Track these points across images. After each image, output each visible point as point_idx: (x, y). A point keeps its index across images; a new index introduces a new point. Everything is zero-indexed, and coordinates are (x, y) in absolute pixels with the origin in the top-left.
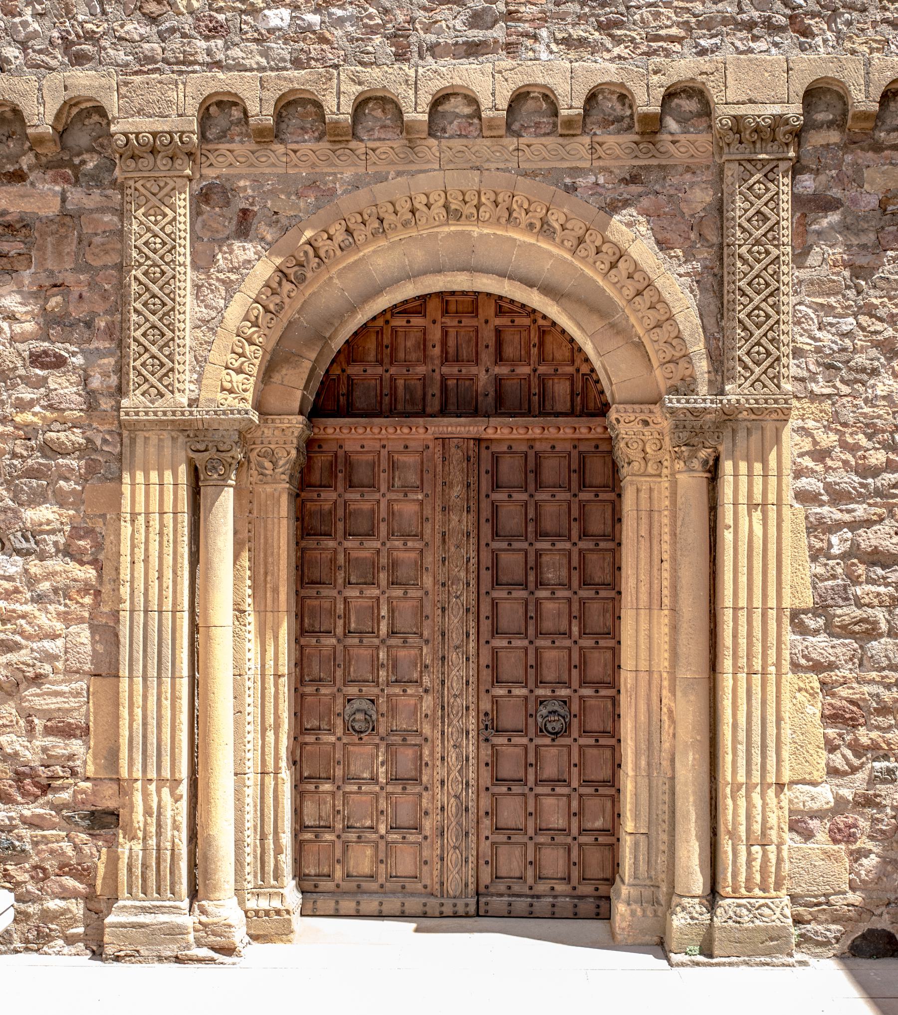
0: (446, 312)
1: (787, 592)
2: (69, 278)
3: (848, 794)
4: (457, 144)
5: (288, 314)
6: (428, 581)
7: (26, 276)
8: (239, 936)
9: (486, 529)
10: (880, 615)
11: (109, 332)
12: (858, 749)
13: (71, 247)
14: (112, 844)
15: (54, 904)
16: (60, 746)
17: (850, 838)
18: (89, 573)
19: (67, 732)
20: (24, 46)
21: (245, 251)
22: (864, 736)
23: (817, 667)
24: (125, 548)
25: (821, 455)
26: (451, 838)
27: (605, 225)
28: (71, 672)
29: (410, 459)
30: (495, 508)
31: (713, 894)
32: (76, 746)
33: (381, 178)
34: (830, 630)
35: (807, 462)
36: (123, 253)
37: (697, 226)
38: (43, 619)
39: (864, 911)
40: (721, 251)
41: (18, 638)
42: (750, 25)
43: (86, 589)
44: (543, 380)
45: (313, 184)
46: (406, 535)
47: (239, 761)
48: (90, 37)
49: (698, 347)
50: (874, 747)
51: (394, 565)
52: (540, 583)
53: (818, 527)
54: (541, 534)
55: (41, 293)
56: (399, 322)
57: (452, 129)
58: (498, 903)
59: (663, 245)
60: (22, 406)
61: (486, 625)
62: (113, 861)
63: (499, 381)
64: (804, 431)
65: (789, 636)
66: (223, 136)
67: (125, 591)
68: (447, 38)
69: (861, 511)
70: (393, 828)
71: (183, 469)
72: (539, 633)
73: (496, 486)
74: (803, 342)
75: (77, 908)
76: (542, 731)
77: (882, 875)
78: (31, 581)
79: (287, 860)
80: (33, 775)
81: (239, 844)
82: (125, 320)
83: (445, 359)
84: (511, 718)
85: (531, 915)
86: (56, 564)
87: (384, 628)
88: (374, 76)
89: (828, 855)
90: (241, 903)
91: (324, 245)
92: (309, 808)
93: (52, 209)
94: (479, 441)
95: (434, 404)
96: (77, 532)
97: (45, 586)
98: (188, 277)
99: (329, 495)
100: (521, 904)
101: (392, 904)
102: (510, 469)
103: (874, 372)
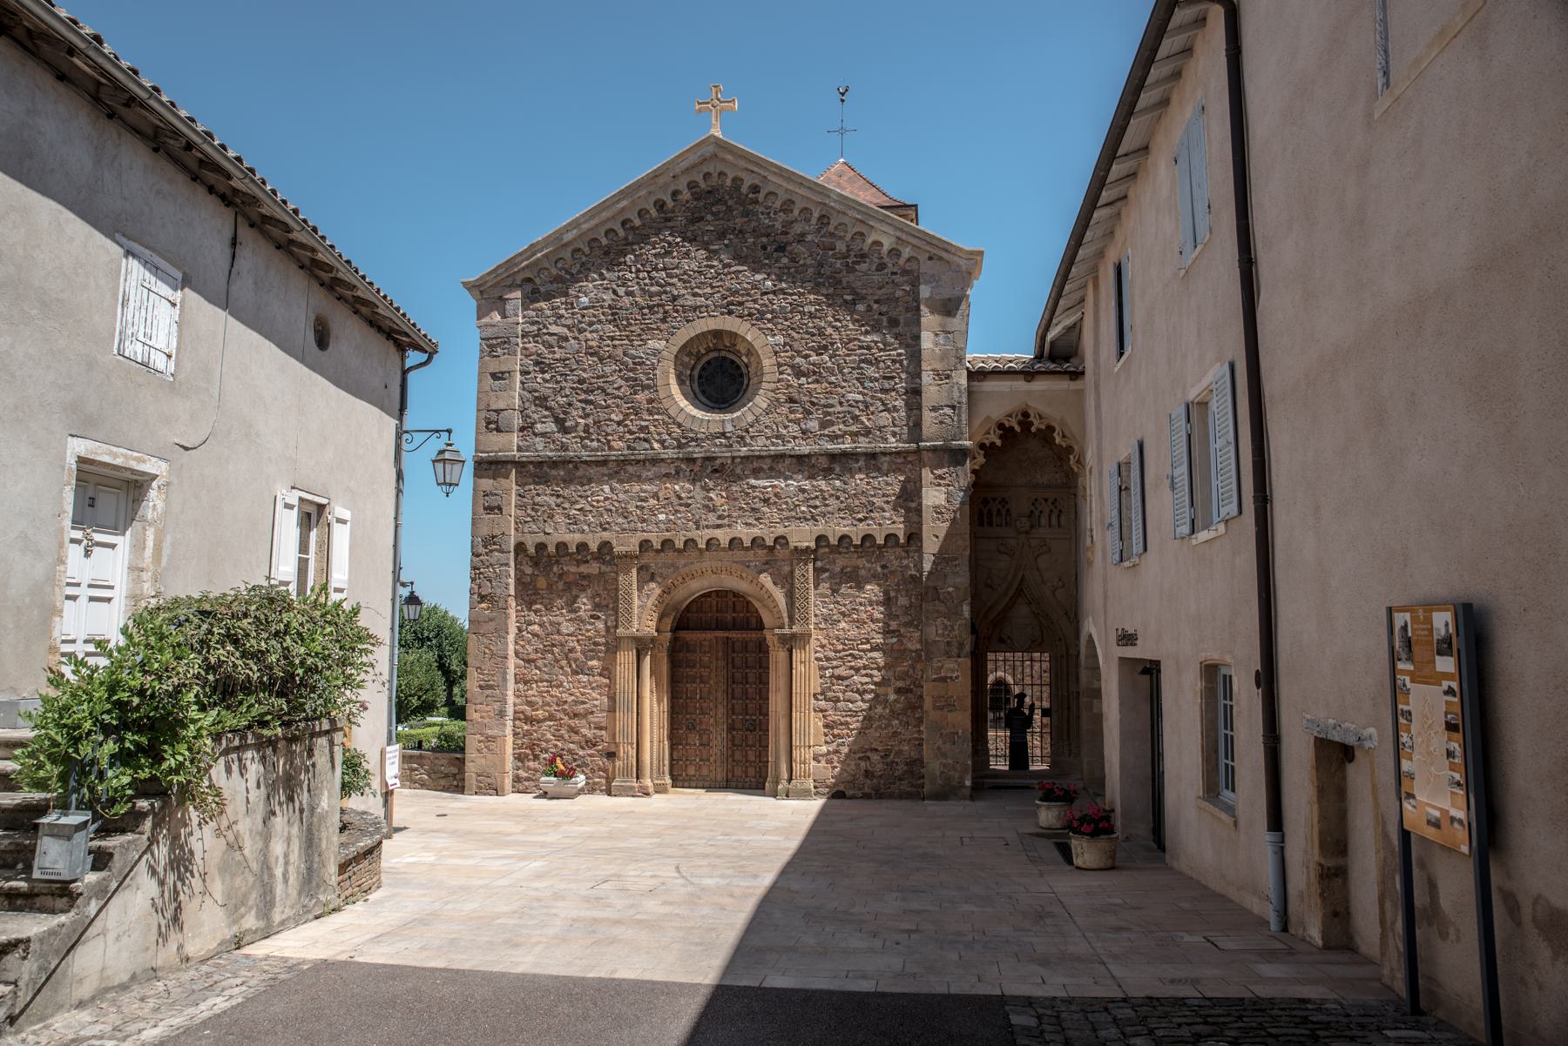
0: (718, 596)
1: (812, 687)
2: (602, 593)
3: (831, 749)
4: (715, 553)
5: (666, 601)
6: (712, 682)
7: (589, 591)
8: (651, 790)
9: (730, 666)
10: (841, 695)
11: (613, 609)
12: (834, 736)
13: (602, 583)
14: (614, 762)
15: (597, 780)
16: (599, 733)
17: (832, 763)
18: (608, 681)
19: (601, 728)
20: (589, 525)
21: (653, 585)
22: (836, 732)
23: (822, 711)
24: (618, 674)
25: (823, 646)
26: (718, 764)
27: (758, 577)
28: (602, 711)
29: (706, 643)
30: (733, 659)
31: (790, 780)
32: (603, 732)
33: (692, 563)
34: (825, 700)
35: (819, 649)
36: (617, 585)
37: (786, 578)
38: (594, 695)
39: (835, 785)
40: (792, 584)
41: (346, 875)
42: (800, 519)
43: (606, 686)
44: (747, 618)
45: (672, 565)
46: (704, 668)
47: (652, 738)
48: (608, 523)
49: (785, 615)
50: (839, 735)
51: (701, 676)
52: (747, 683)
53: (822, 668)
54: (747, 667)
55: (593, 597)
56: (703, 599)
57: (714, 548)
58: (734, 784)
59: (775, 584)
60: (588, 631)
61: (730, 696)
62: (614, 767)
63: (734, 618)
64: (818, 639)
65: (813, 701)
66: (646, 551)
67: (618, 687)
68: (711, 523)
69: (835, 663)
70: (701, 760)
71: (634, 651)
72: (747, 698)
73: (733, 651)
74: (818, 612)
75: (604, 781)
76: (748, 729)
77: (841, 774)
78: (590, 683)
79: (667, 769)
80: (591, 741)
81: (651, 763)
82: (618, 606)
83: (717, 611)
84: (738, 725)
85: (743, 788)
86: (597, 678)
87: (698, 697)
88: (690, 535)
89: (825, 768)
90: (652, 781)
91: (676, 583)
92: (675, 754)
93: (597, 572)
94: (727, 638)
95: (714, 626)
96: (604, 669)
97: (594, 685)
98: (636, 593)
99: (681, 655)
100: (740, 785)
101: (700, 784)
102: (738, 646)
103: (839, 621)
